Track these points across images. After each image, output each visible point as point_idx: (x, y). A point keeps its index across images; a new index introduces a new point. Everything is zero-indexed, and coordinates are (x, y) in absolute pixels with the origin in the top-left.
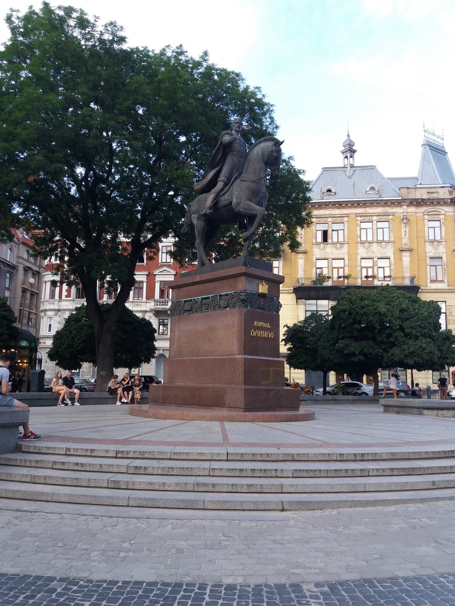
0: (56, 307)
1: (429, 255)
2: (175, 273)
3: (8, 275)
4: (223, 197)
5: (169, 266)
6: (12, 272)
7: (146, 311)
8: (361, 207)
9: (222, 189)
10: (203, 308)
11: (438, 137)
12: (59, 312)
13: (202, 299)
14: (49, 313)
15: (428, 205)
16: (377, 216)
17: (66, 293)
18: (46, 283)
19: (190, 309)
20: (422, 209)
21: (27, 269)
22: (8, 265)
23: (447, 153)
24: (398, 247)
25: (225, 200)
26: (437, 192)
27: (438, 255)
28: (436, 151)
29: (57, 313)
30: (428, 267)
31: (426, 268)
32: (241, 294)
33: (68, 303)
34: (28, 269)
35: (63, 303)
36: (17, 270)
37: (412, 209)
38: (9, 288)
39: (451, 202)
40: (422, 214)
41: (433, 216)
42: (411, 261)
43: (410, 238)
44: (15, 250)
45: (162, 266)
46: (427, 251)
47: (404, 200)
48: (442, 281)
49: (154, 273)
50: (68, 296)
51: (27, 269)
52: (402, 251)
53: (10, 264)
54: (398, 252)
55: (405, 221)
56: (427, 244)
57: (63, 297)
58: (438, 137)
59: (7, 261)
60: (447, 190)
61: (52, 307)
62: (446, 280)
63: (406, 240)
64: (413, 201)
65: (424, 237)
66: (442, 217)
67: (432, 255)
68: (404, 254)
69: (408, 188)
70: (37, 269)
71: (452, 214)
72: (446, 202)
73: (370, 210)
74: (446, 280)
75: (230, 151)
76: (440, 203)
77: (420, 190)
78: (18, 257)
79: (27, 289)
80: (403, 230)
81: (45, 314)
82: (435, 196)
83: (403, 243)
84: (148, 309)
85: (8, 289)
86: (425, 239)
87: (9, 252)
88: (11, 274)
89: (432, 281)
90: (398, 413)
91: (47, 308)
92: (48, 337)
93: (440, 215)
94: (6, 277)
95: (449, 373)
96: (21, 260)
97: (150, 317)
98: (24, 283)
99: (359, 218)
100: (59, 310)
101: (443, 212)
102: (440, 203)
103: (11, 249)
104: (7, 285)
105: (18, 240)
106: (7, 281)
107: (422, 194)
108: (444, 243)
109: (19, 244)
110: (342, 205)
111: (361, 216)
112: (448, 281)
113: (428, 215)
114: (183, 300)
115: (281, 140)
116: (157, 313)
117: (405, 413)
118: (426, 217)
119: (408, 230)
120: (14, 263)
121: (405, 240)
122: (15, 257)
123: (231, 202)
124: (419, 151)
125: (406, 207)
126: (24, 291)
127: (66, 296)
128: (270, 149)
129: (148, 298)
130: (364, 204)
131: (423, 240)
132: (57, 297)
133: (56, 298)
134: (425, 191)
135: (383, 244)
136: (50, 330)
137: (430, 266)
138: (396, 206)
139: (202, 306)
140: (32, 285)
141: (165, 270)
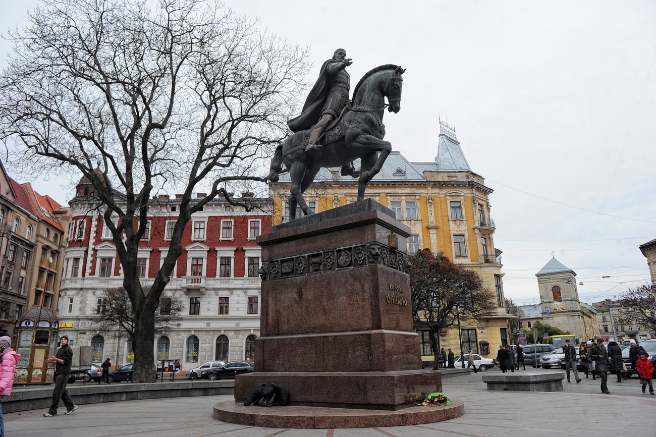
0: (79, 286)
1: (452, 232)
2: (208, 249)
3: (25, 254)
4: (330, 132)
5: (202, 242)
6: (30, 251)
7: (176, 290)
8: (390, 187)
9: (329, 123)
10: (311, 269)
11: (451, 129)
12: (81, 291)
13: (309, 256)
14: (70, 293)
15: (449, 187)
16: (391, 196)
17: (90, 271)
18: (68, 260)
19: (290, 271)
20: (444, 191)
21: (45, 249)
22: (26, 243)
23: (459, 143)
24: (426, 225)
25: (335, 135)
26: (456, 176)
27: (460, 233)
28: (450, 140)
29: (79, 292)
30: (453, 244)
31: (451, 245)
32: (372, 247)
33: (91, 281)
34: (47, 248)
35: (86, 282)
36: (36, 249)
37: (436, 191)
38: (25, 267)
39: (469, 185)
40: (444, 195)
41: (454, 197)
42: (438, 238)
43: (435, 217)
44: (35, 228)
45: (195, 242)
46: (451, 229)
47: (429, 182)
48: (466, 257)
49: (186, 250)
50: (93, 273)
51: (45, 249)
52: (428, 228)
53: (28, 242)
54: (425, 229)
55: (430, 201)
56: (451, 222)
57: (87, 275)
58: (451, 129)
59: (25, 239)
60: (464, 174)
61: (74, 286)
62: (469, 256)
63: (432, 218)
64: (436, 183)
65: (448, 216)
66: (462, 198)
67: (455, 232)
68: (431, 231)
69: (431, 171)
70: (56, 248)
71: (470, 195)
72: (465, 185)
73: (399, 191)
74: (469, 256)
75: (337, 82)
76: (459, 185)
77: (442, 174)
78: (38, 235)
79: (45, 269)
80: (429, 209)
81: (65, 293)
82: (454, 179)
83: (430, 221)
84: (179, 287)
85: (25, 268)
86: (449, 218)
87: (28, 230)
88: (28, 253)
89: (457, 257)
90: (505, 389)
91: (68, 286)
92: (67, 319)
93: (460, 196)
94: (23, 256)
95: (477, 344)
96: (40, 239)
97: (181, 295)
98: (41, 262)
99: (389, 198)
100: (82, 289)
101: (463, 194)
102: (459, 185)
103: (30, 227)
104: (23, 265)
105: (39, 218)
106: (24, 259)
107: (443, 178)
108: (465, 222)
109: (40, 221)
110: (373, 185)
111: (391, 196)
112: (471, 257)
113: (450, 196)
114: (279, 259)
115: (404, 69)
116: (188, 291)
117: (515, 390)
118: (448, 198)
119: (433, 210)
120: (33, 241)
121: (432, 219)
122: (34, 235)
123: (344, 136)
124: (437, 139)
125: (430, 188)
126: (41, 271)
127: (90, 274)
128: (391, 77)
129: (179, 276)
130: (393, 185)
131: (447, 219)
132: (80, 275)
133: (78, 276)
134: (446, 174)
135: (413, 222)
136: (70, 311)
137: (455, 242)
138: (421, 188)
139: (309, 266)
140: (50, 265)
141: (198, 246)
